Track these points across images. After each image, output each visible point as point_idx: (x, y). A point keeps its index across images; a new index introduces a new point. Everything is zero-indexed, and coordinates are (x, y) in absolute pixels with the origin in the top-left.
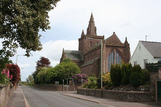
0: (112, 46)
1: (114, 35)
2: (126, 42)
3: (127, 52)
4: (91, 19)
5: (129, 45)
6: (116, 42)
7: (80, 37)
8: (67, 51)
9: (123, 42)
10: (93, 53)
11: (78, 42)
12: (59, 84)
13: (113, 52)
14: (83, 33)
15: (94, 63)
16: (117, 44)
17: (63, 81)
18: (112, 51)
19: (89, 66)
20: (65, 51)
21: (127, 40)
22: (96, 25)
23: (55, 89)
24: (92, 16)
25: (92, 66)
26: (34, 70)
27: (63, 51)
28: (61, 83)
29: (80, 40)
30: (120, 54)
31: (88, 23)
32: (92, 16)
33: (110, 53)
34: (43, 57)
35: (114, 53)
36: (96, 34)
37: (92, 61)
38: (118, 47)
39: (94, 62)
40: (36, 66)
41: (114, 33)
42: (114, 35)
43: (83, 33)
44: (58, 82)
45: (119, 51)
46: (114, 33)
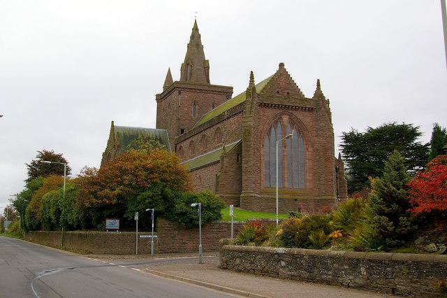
0: (277, 106)
1: (282, 73)
2: (319, 94)
3: (324, 124)
4: (192, 37)
5: (328, 102)
6: (288, 93)
7: (161, 91)
8: (124, 128)
9: (309, 93)
10: (208, 133)
11: (154, 106)
12: (122, 228)
13: (279, 125)
14: (169, 75)
15: (223, 160)
16: (293, 101)
17: (136, 218)
18: (276, 122)
19: (205, 170)
20: (119, 128)
21: (322, 88)
22: (208, 54)
23: (107, 248)
24: (196, 29)
25: (216, 169)
26: (21, 187)
27: (113, 126)
28: (127, 225)
29: (160, 98)
30: (301, 131)
31: (185, 50)
32: (196, 29)
33: (273, 129)
34: (46, 153)
35: (283, 127)
36: (208, 81)
37: (215, 154)
38: (296, 108)
39: (223, 158)
40: (27, 177)
41: (281, 65)
42: (282, 73)
43: (169, 75)
44: (118, 221)
45: (300, 122)
46: (281, 65)
